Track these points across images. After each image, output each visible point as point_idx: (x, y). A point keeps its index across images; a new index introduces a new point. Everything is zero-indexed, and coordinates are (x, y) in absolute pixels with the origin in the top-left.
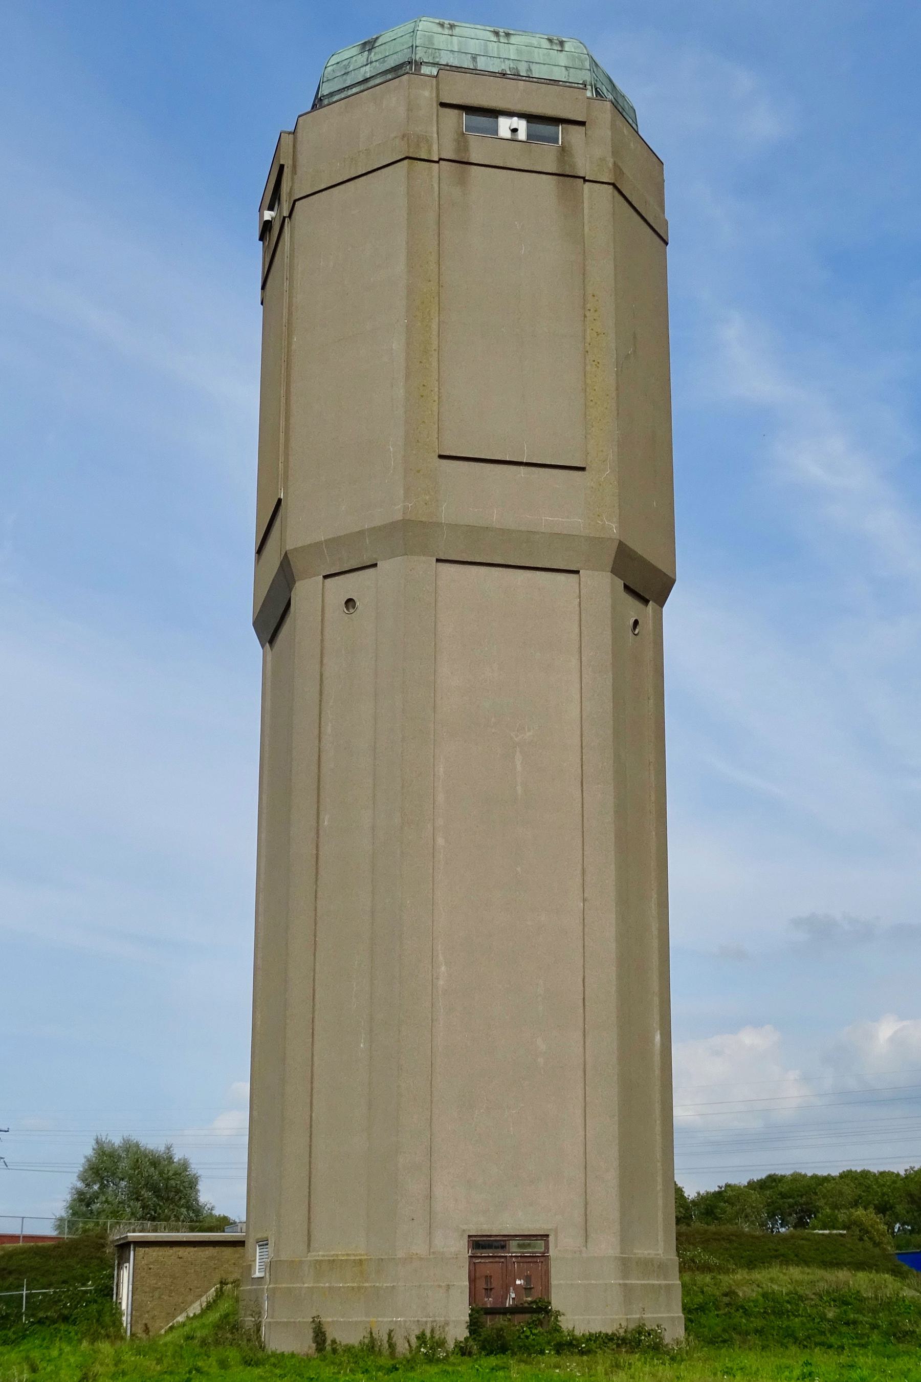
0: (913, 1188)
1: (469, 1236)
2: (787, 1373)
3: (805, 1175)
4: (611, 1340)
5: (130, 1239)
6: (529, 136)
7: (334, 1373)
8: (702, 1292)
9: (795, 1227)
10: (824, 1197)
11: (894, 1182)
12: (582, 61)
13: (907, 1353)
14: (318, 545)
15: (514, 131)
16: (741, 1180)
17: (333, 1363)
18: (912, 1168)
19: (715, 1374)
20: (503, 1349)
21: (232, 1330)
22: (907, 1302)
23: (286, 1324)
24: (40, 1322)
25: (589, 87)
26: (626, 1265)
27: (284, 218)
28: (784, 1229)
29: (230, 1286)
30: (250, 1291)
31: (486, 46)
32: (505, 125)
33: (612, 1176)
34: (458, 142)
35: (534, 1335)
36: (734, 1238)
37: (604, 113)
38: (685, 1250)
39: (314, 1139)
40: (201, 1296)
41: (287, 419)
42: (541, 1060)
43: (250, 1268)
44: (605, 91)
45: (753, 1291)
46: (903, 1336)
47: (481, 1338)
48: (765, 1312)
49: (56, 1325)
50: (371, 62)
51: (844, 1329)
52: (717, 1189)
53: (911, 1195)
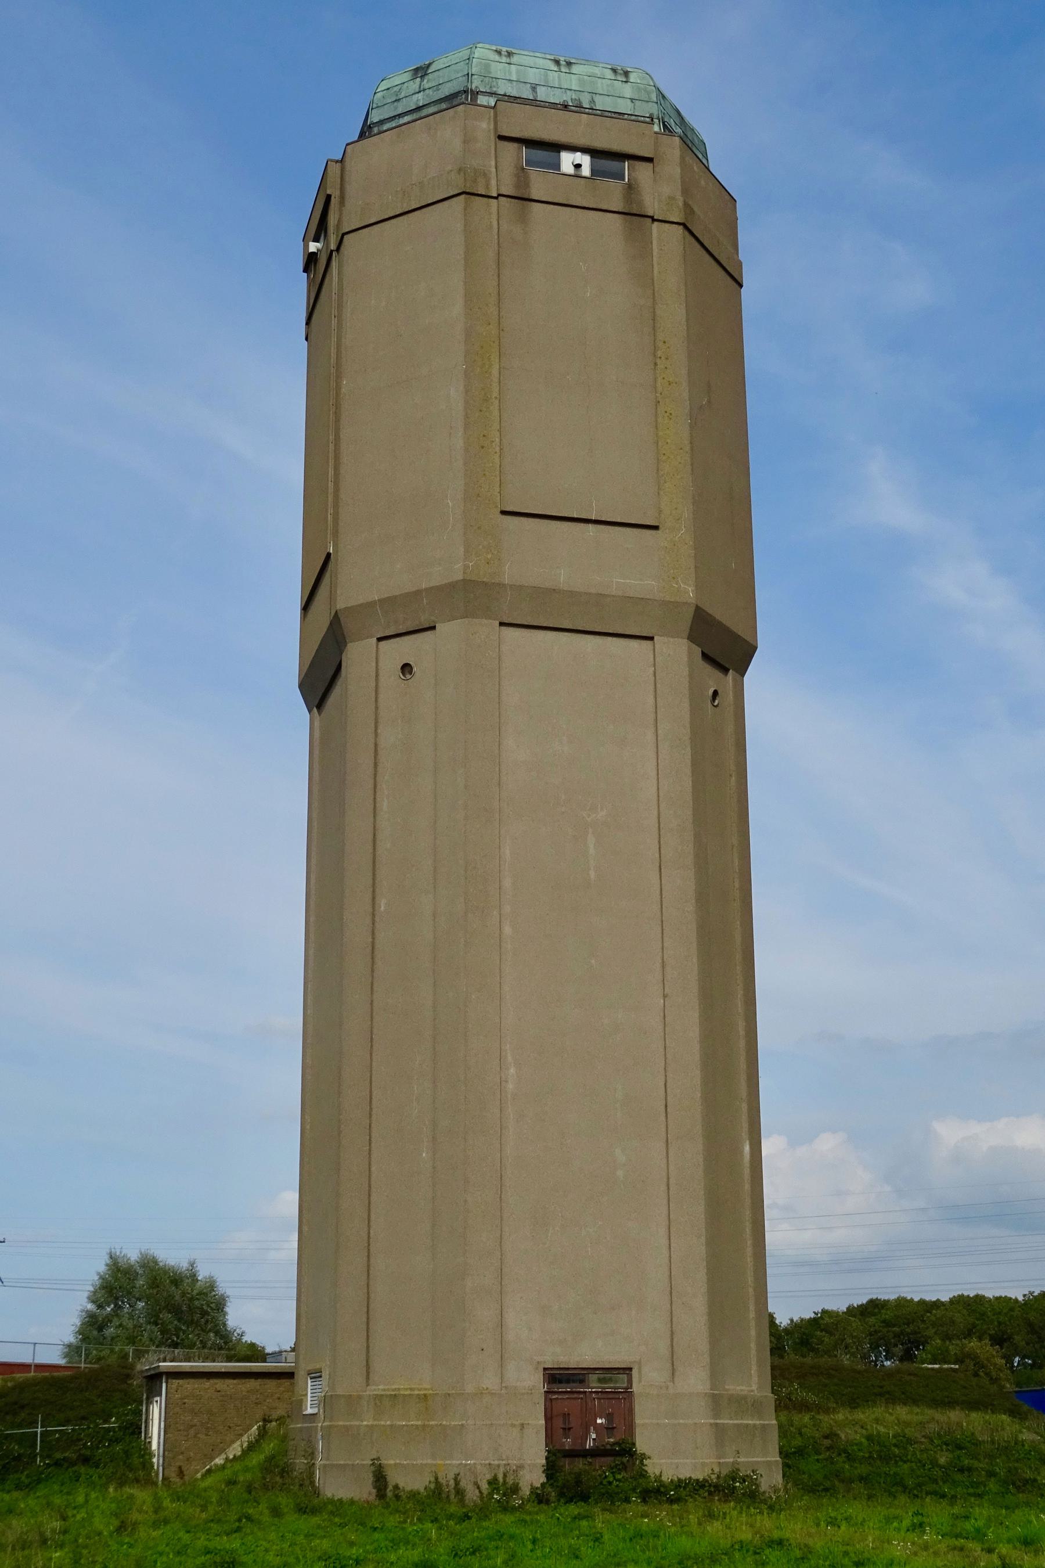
0: (1032, 1316)
1: (545, 1369)
2: (895, 1524)
3: (912, 1300)
4: (703, 1486)
5: (162, 1370)
6: (593, 171)
7: (400, 1522)
8: (800, 1434)
9: (901, 1360)
10: (934, 1325)
11: (1012, 1310)
12: (649, 93)
13: (1027, 1504)
14: (371, 605)
15: (578, 166)
16: (840, 1305)
17: (397, 1511)
18: (1031, 1293)
19: (818, 1525)
20: (584, 1498)
21: (280, 1477)
22: (1026, 1447)
23: (343, 1467)
24: (57, 1464)
25: (656, 121)
26: (717, 1402)
27: (332, 251)
28: (889, 1363)
29: (274, 1423)
30: (301, 1429)
31: (546, 76)
32: (567, 161)
33: (700, 1304)
34: (517, 176)
35: (617, 1480)
36: (833, 1372)
37: (673, 147)
38: (780, 1386)
39: (372, 1261)
40: (242, 1435)
41: (336, 468)
42: (620, 1173)
43: (300, 1403)
44: (673, 124)
45: (856, 1432)
46: (1025, 1485)
47: (560, 1484)
48: (870, 1457)
49: (75, 1468)
50: (424, 90)
51: (958, 1477)
52: (813, 1316)
53: (1030, 1325)
